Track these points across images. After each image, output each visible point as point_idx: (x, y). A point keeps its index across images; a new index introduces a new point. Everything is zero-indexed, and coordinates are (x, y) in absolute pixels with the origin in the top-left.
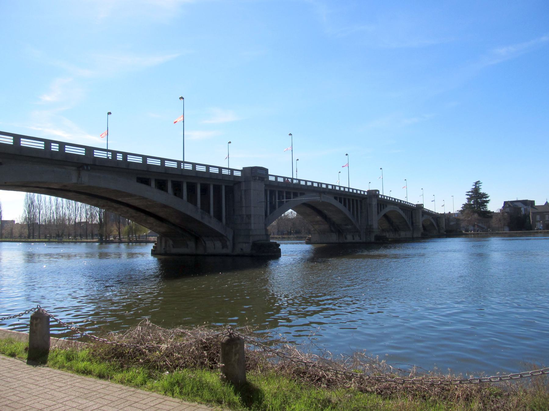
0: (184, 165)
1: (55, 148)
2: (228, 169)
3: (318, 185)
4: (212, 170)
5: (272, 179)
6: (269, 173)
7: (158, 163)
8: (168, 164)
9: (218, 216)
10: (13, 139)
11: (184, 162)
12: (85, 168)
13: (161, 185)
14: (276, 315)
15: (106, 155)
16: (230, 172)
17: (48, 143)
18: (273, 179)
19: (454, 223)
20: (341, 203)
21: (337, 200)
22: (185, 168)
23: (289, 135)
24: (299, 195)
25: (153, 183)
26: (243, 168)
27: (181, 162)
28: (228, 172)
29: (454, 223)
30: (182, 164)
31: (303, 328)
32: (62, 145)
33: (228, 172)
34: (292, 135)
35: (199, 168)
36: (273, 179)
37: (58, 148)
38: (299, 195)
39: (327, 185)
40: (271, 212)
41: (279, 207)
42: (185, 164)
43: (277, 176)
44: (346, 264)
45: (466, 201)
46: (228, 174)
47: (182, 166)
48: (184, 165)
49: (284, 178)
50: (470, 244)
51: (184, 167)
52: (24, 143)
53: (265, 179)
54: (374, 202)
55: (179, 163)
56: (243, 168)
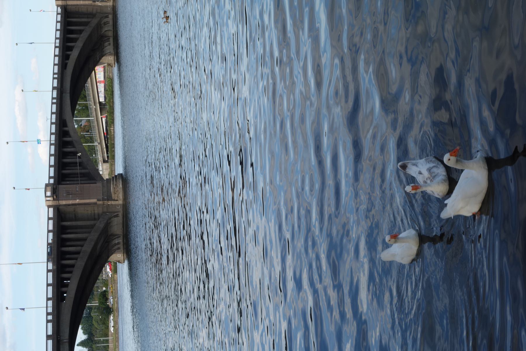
1: (50, 317)
2: (52, 91)
6: (48, 183)
7: (52, 158)
8: (53, 152)
9: (86, 24)
10: (49, 272)
12: (59, 339)
14: (202, 240)
15: (50, 308)
16: (55, 90)
17: (48, 321)
18: (56, 67)
20: (74, 47)
23: (7, 144)
24: (66, 129)
31: (241, 264)
33: (55, 92)
36: (56, 67)
38: (66, 129)
43: (47, 271)
44: (152, 75)
46: (51, 308)
49: (49, 232)
50: (403, 244)
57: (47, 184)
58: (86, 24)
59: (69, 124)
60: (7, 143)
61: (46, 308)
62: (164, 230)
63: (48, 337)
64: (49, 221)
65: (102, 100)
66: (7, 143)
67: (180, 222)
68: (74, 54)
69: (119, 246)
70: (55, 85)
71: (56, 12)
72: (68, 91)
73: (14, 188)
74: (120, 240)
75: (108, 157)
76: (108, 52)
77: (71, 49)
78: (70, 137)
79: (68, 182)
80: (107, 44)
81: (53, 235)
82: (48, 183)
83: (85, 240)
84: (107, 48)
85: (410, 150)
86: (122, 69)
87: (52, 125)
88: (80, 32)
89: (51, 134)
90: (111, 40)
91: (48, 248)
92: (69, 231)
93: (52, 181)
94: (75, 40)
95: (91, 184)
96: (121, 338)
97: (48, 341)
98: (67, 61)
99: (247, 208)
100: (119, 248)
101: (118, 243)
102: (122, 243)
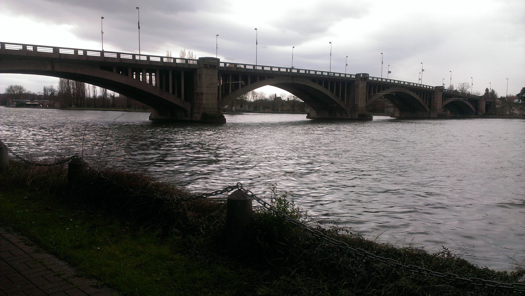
0: (256, 67)
1: (81, 53)
2: (376, 78)
3: (398, 82)
4: (342, 75)
5: (222, 65)
6: (369, 76)
9: (343, 99)
11: (257, 66)
13: (320, 83)
17: (76, 50)
19: (500, 106)
21: (316, 83)
22: (141, 59)
23: (136, 8)
25: (317, 82)
26: (199, 58)
27: (255, 65)
28: (181, 61)
29: (500, 106)
30: (189, 61)
32: (85, 51)
33: (181, 61)
34: (139, 8)
35: (282, 70)
37: (146, 58)
39: (404, 82)
40: (223, 96)
41: (233, 90)
42: (141, 56)
43: (309, 70)
45: (519, 93)
47: (189, 62)
48: (256, 67)
51: (256, 68)
52: (39, 50)
53: (217, 67)
54: (362, 86)
55: (254, 66)
56: (199, 58)
57: (219, 60)
60: (330, 43)
61: (139, 54)
62: (399, 142)
63: (56, 49)
64: (224, 64)
65: (144, 117)
66: (330, 43)
67: (254, 179)
70: (301, 72)
71: (387, 78)
81: (20, 50)
87: (224, 64)
89: (263, 67)
97: (160, 58)
99: (344, 217)
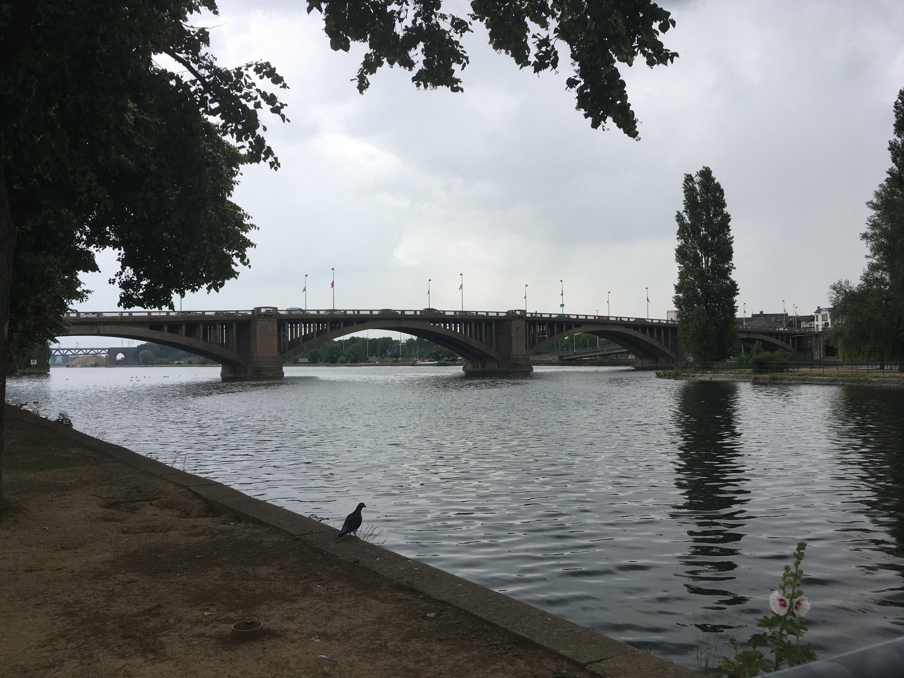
6: (527, 312)
8: (500, 314)
24: (355, 324)
38: (355, 324)
58: (666, 344)
59: (577, 329)
68: (639, 335)
69: (476, 367)
72: (606, 329)
73: (527, 286)
74: (480, 369)
75: (564, 360)
76: (644, 362)
77: (644, 331)
78: (566, 330)
79: (528, 328)
80: (650, 361)
82: (527, 312)
83: (481, 341)
84: (647, 362)
85: (574, 578)
86: (627, 373)
88: (659, 340)
90: (654, 365)
91: (94, 313)
92: (488, 328)
93: (528, 315)
94: (652, 335)
95: (525, 346)
96: (724, 379)
98: (632, 329)
100: (474, 367)
101: (478, 367)
102: (478, 369)
